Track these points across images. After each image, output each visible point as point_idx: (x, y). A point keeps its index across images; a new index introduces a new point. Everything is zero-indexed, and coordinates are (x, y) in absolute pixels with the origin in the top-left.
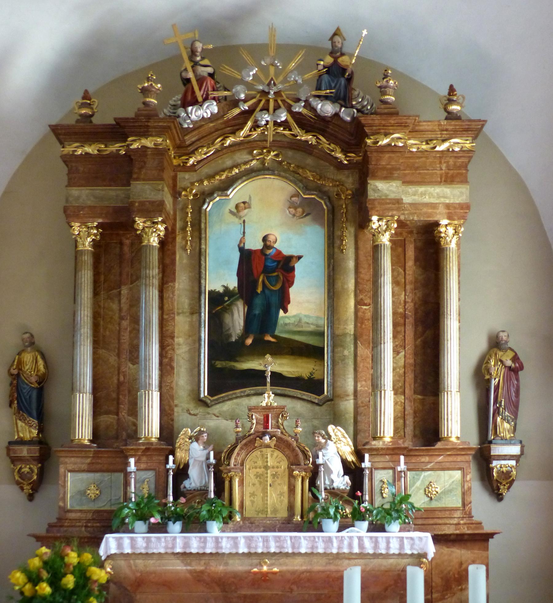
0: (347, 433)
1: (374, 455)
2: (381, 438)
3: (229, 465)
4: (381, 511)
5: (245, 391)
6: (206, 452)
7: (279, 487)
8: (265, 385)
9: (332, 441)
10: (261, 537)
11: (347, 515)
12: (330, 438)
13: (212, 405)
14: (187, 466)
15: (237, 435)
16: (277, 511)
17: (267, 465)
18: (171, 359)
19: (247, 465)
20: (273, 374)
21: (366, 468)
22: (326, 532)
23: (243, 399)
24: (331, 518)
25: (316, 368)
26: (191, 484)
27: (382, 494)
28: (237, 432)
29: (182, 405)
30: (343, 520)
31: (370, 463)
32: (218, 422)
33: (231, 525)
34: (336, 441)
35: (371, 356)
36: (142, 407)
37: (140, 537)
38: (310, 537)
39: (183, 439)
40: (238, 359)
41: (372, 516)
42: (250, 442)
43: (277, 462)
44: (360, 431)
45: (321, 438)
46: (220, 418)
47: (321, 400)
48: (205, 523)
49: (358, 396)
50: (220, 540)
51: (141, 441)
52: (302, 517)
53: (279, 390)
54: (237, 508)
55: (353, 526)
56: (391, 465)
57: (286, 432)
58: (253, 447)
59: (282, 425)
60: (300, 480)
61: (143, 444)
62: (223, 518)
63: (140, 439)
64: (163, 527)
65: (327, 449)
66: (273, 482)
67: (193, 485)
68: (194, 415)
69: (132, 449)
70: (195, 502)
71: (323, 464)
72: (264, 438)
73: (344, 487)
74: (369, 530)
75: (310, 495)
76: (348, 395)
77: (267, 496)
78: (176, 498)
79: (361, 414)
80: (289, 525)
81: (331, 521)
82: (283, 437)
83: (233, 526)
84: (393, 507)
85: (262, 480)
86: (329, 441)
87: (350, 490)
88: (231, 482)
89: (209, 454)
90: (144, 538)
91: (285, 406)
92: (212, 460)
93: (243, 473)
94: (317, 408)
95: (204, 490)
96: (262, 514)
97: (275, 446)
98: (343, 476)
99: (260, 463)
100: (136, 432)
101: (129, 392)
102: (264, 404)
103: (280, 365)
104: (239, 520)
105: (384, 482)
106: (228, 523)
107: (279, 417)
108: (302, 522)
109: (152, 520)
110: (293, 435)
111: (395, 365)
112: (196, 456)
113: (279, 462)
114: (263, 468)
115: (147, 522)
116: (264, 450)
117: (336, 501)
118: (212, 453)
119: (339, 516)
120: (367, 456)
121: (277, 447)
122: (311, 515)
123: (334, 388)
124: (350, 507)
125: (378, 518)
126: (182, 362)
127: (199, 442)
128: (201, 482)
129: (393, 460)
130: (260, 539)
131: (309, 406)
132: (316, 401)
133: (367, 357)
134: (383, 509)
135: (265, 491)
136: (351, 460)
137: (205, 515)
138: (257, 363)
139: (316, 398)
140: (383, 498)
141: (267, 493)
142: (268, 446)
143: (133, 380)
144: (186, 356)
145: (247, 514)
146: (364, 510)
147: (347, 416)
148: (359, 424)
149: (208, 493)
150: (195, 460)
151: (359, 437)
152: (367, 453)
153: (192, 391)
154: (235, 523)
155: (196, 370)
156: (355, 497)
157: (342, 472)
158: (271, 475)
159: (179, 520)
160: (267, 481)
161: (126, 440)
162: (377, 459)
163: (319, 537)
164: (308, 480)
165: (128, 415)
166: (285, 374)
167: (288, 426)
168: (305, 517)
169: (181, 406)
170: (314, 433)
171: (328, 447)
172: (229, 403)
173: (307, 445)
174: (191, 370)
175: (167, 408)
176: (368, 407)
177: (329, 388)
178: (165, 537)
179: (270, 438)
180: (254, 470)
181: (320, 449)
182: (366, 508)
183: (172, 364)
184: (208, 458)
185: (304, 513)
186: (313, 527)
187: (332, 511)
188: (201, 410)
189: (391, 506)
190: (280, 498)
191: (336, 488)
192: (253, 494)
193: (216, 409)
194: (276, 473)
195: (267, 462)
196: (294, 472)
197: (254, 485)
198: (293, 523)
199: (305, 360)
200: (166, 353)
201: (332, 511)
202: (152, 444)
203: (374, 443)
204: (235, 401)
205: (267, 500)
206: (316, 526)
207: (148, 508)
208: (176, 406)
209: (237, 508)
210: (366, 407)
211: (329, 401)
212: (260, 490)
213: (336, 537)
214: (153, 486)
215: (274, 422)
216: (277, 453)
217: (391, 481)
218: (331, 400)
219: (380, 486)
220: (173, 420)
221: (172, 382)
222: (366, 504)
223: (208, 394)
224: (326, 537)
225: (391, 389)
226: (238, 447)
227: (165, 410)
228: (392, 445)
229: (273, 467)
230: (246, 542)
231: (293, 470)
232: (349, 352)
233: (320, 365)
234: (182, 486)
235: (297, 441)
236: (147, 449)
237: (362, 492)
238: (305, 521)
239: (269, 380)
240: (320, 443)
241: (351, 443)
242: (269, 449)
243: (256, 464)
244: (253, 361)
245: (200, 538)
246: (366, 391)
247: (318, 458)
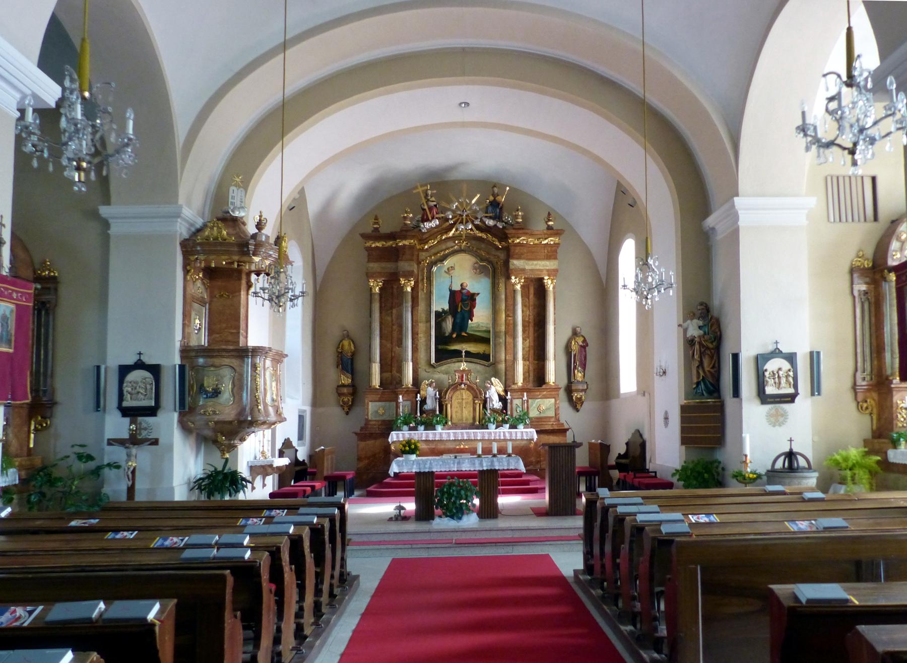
12: (492, 384)
14: (425, 398)
18: (417, 345)
19: (454, 398)
33: (446, 426)
52: (479, 422)
53: (468, 359)
61: (405, 388)
92: (438, 396)
99: (460, 397)
109: (411, 425)
118: (437, 393)
122: (484, 421)
131: (483, 367)
135: (462, 410)
142: (463, 389)
144: (424, 343)
145: (454, 421)
153: (428, 360)
166: (472, 352)
181: (488, 390)
184: (436, 395)
187: (492, 420)
201: (492, 420)
202: (409, 388)
203: (513, 386)
214: (410, 408)
216: (467, 392)
236: (407, 391)
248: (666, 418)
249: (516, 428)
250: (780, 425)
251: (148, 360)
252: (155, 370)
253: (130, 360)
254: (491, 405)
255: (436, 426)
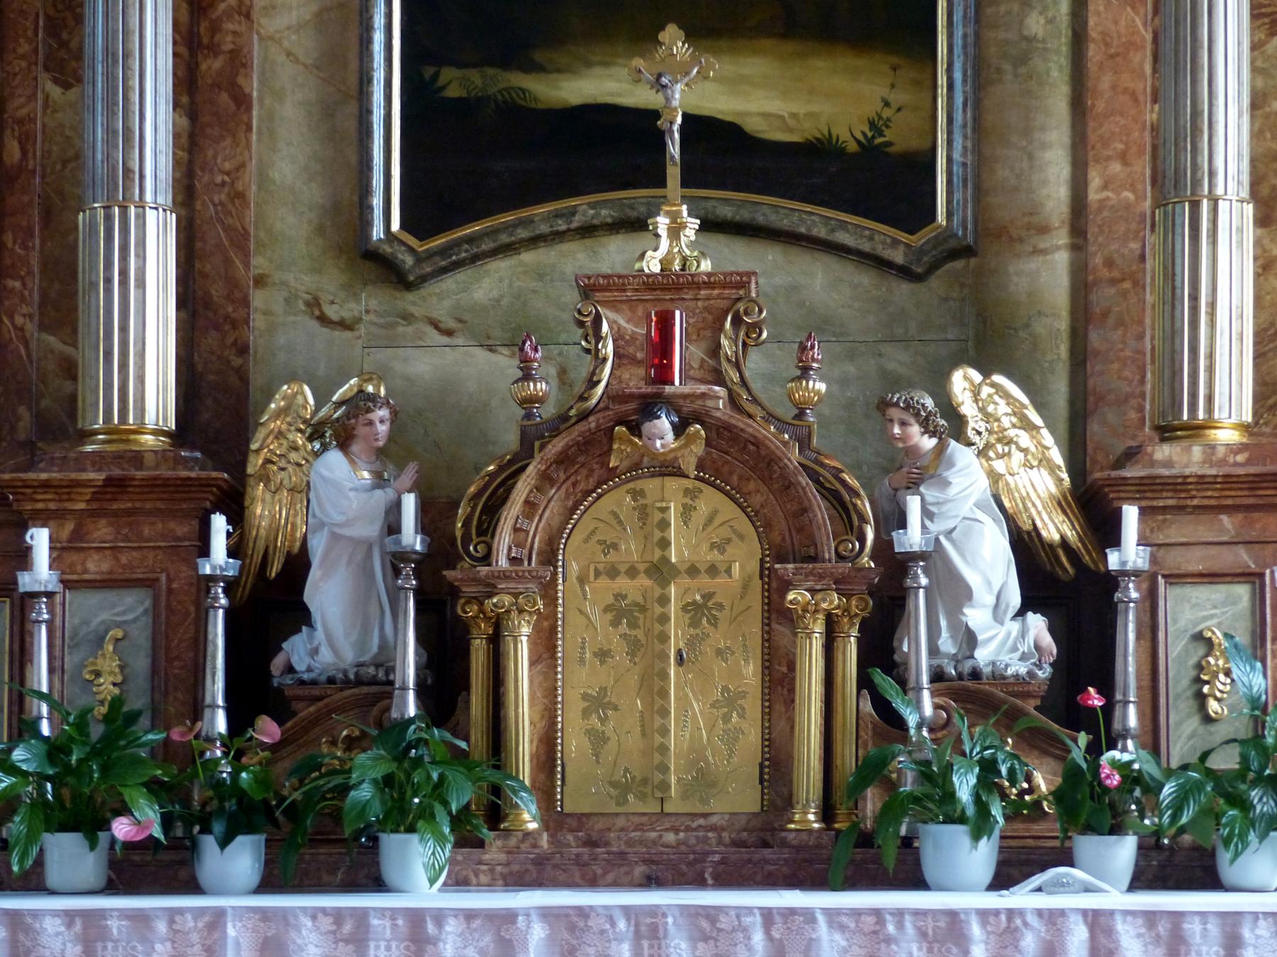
0: (1039, 407)
1: (1164, 509)
2: (1196, 430)
3: (486, 559)
4: (1199, 787)
5: (573, 212)
6: (382, 497)
7: (719, 667)
8: (662, 183)
9: (970, 444)
10: (627, 910)
11: (1037, 804)
12: (956, 426)
13: (423, 279)
14: (298, 565)
15: (529, 416)
16: (713, 785)
17: (665, 560)
18: (238, 61)
19: (572, 563)
20: (696, 126)
21: (1124, 573)
22: (941, 888)
23: (567, 247)
24: (962, 820)
25: (897, 97)
26: (315, 652)
27: (1201, 699)
28: (528, 402)
29: (290, 277)
30: (1020, 828)
31: (1145, 552)
32: (450, 355)
33: (495, 850)
34: (988, 446)
35: (1149, 37)
36: (94, 285)
37: (55, 913)
38: (856, 913)
39: (280, 435)
40: (539, 56)
41: (1157, 809)
42: (585, 445)
43: (713, 546)
44: (1101, 398)
45: (915, 429)
46: (459, 341)
47: (921, 252)
48: (375, 840)
49: (1092, 230)
50: (431, 928)
51: (89, 448)
52: (827, 814)
53: (728, 202)
54: (526, 772)
55: (1066, 858)
56: (1245, 558)
57: (755, 401)
58: (599, 473)
59: (737, 366)
60: (819, 628)
61: (99, 460)
62: (458, 821)
63: (86, 435)
64: (182, 863)
65: (947, 484)
66: (691, 643)
67: (326, 656)
68: (344, 325)
69: (46, 485)
70: (333, 743)
71: (922, 556)
72: (647, 427)
73: (1023, 670)
74: (1142, 880)
75: (867, 707)
76: (1044, 230)
77: (665, 712)
78: (239, 720)
79: (1105, 314)
80: (767, 853)
81: (960, 832)
82: (739, 421)
83: (503, 857)
84: (1255, 765)
85: (639, 633)
86: (953, 443)
87: (1052, 679)
88: (495, 641)
89: (395, 509)
90: (69, 916)
91: (750, 274)
92: (411, 538)
93: (551, 601)
94: (903, 290)
95: (373, 682)
96: (642, 797)
97: (700, 467)
98: (1021, 613)
99: (631, 549)
100: (72, 412)
101: (48, 216)
102: (652, 264)
103: (734, 83)
104: (533, 826)
105: (1209, 643)
106: (480, 844)
107: (721, 328)
108: (827, 838)
109: (122, 828)
110: (788, 413)
111: (1260, 83)
112: (338, 518)
113: (720, 547)
114: (647, 572)
115: (102, 836)
116: (651, 486)
117: (984, 735)
118: (410, 503)
119: (997, 810)
120: (1131, 515)
121: (711, 473)
122: (872, 802)
123: (980, 192)
124: (1051, 763)
125: (1184, 820)
126: (286, 73)
127: (355, 448)
128: (361, 644)
129: (1254, 535)
130: (622, 925)
131: (865, 279)
132: (898, 257)
133: (1132, 45)
134: (1210, 773)
135: (654, 688)
136: (1057, 537)
137: (365, 805)
138: (623, 72)
139: (895, 243)
140: (1208, 719)
141: (664, 694)
142: (668, 468)
143: (65, 163)
144: (306, 45)
145: (572, 801)
146: (1116, 780)
147: (1039, 327)
148: (1094, 367)
149: (390, 696)
150: (335, 538)
151: (1095, 428)
152: (1131, 500)
153: (335, 209)
154: (513, 842)
155: (352, 108)
156: (1077, 717)
157: (1014, 598)
158: (685, 609)
159: (250, 830)
160: (664, 638)
161: (30, 446)
162: (1179, 530)
163: (899, 914)
164: (855, 632)
165: (43, 327)
166: (754, 126)
167: (770, 378)
168: (841, 811)
169: (285, 284)
170: (884, 405)
171: (951, 475)
172: (501, 267)
173: (855, 469)
174: (327, 111)
175: (217, 291)
176: (1138, 285)
177: (957, 196)
178: (172, 913)
179: (679, 430)
180: (604, 581)
181: (913, 485)
182: (1124, 767)
183: (241, 80)
184: (393, 528)
185: (839, 794)
186: (877, 860)
187: (964, 786)
188: (373, 304)
189: (1244, 759)
190: (726, 718)
191: (987, 670)
192: (598, 703)
193: (440, 297)
194: (708, 597)
195: (664, 544)
196: (791, 596)
197: (603, 655)
198: (784, 843)
199: (849, 60)
200: (215, 28)
201: (964, 786)
202: (137, 458)
203: (1163, 452)
204: (528, 257)
205: (664, 731)
206: (890, 855)
207: (105, 770)
208: (260, 281)
209: (526, 772)
210: (1127, 285)
211: (954, 254)
212: (634, 679)
213: (985, 915)
214: (141, 663)
215: (698, 352)
216: (710, 500)
217: (1243, 638)
218: (967, 252)
219: (1193, 661)
220: (243, 350)
221: (242, 166)
222: (1128, 753)
223: (404, 225)
224: (934, 913)
225: (1245, 194)
226: (530, 469)
227: (208, 304)
228: (1248, 462)
229: (693, 571)
230: (551, 939)
231: (787, 586)
232: (1051, 21)
233: (917, 83)
234: (277, 664)
235: (804, 443)
236: (115, 486)
237: (1107, 689)
238: (838, 832)
239: (674, 149)
240: (912, 452)
241: (1057, 457)
242: (673, 484)
243: (612, 557)
244: (606, 64)
245: (338, 916)
246: (1128, 206)
247: (902, 524)
249: (1209, 879)
254: (947, 644)
255: (392, 843)
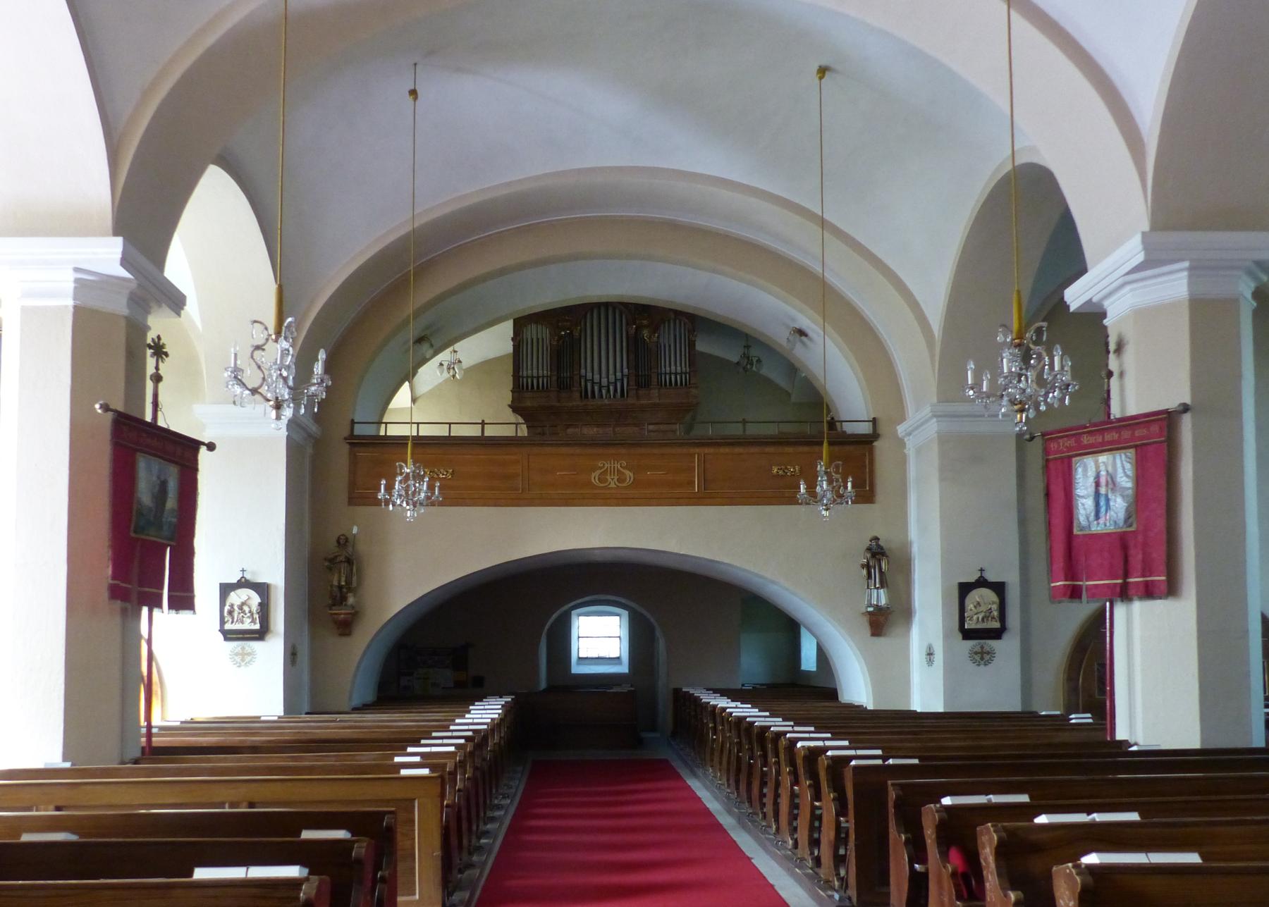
248: (930, 654)
250: (985, 665)
251: (991, 577)
252: (999, 588)
253: (972, 578)
